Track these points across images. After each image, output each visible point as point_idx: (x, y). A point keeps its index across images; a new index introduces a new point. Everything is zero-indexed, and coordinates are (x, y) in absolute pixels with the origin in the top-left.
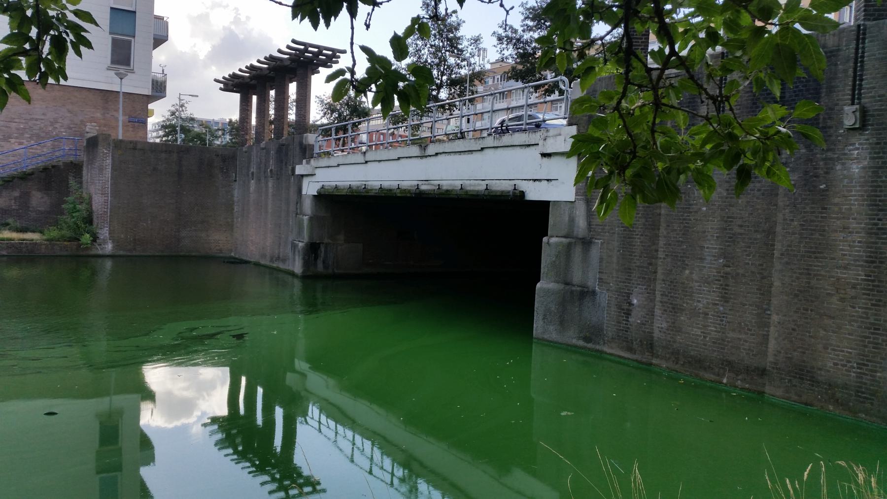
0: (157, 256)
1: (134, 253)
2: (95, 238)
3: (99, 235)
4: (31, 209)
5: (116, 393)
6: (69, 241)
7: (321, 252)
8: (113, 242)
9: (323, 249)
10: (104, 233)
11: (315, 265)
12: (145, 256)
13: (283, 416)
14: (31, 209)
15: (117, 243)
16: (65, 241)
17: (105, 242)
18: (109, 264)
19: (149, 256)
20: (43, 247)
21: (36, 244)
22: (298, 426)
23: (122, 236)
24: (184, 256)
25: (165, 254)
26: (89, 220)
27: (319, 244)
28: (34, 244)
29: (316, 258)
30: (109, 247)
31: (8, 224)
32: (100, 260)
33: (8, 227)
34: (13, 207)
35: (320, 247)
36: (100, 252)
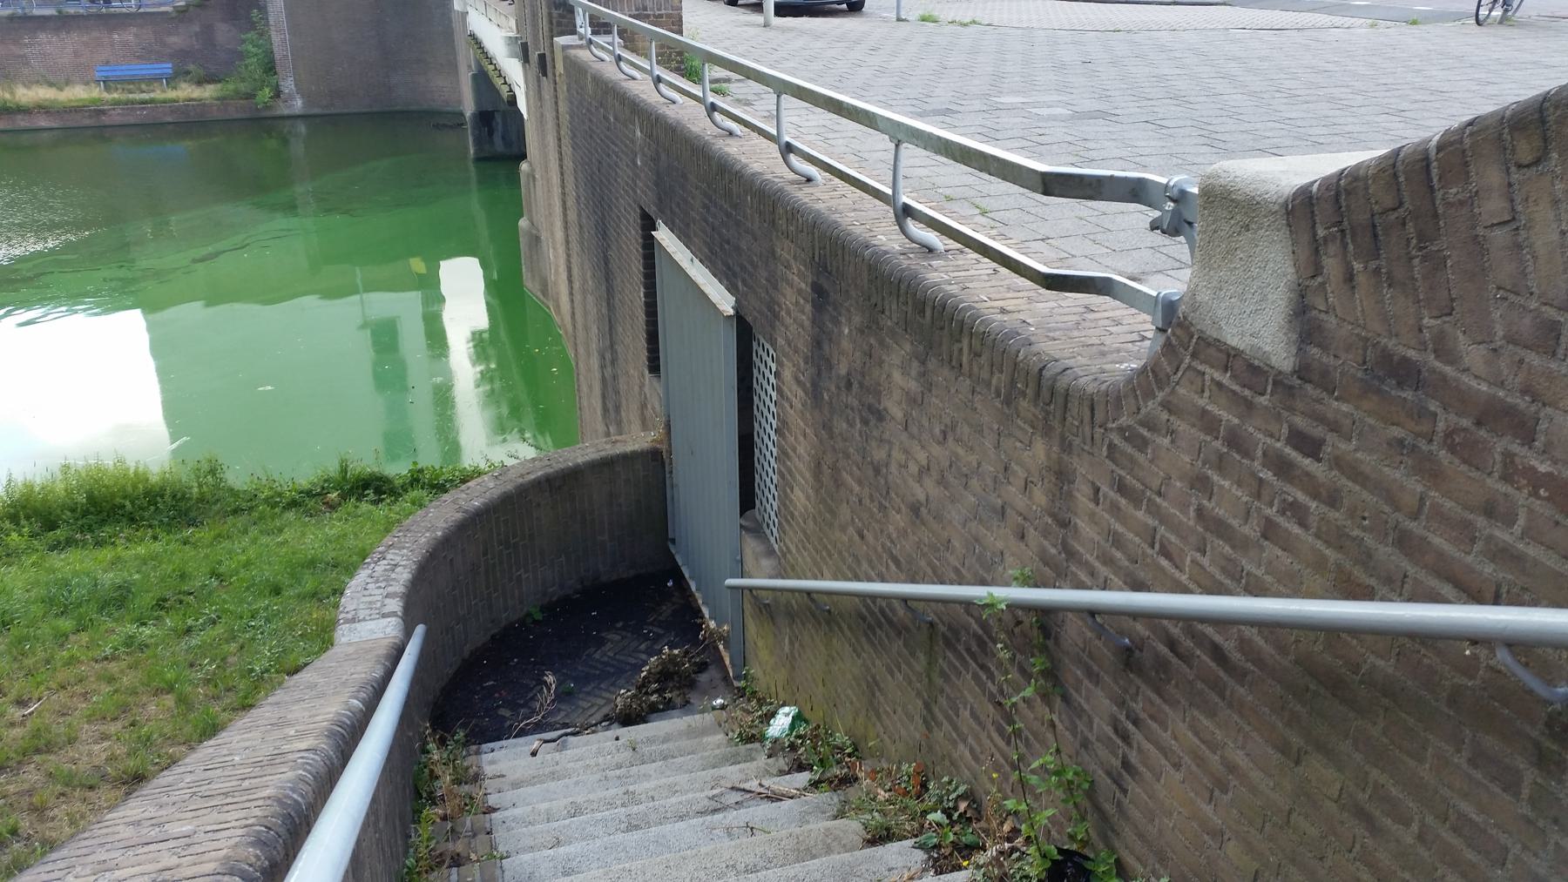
0: (364, 114)
1: (333, 111)
2: (277, 94)
3: (282, 88)
4: (218, 48)
5: (367, 290)
6: (247, 99)
7: (497, 124)
8: (303, 97)
9: (498, 118)
10: (288, 85)
11: (492, 142)
12: (348, 114)
13: (162, 402)
14: (218, 48)
15: (308, 98)
16: (241, 98)
17: (291, 97)
18: (302, 128)
19: (355, 114)
20: (215, 108)
21: (204, 105)
22: (933, 277)
23: (313, 88)
24: (402, 112)
25: (375, 109)
26: (270, 68)
27: (493, 112)
28: (201, 104)
29: (491, 133)
30: (298, 105)
31: (188, 73)
32: (288, 122)
33: (189, 77)
34: (196, 47)
35: (493, 117)
36: (286, 112)
